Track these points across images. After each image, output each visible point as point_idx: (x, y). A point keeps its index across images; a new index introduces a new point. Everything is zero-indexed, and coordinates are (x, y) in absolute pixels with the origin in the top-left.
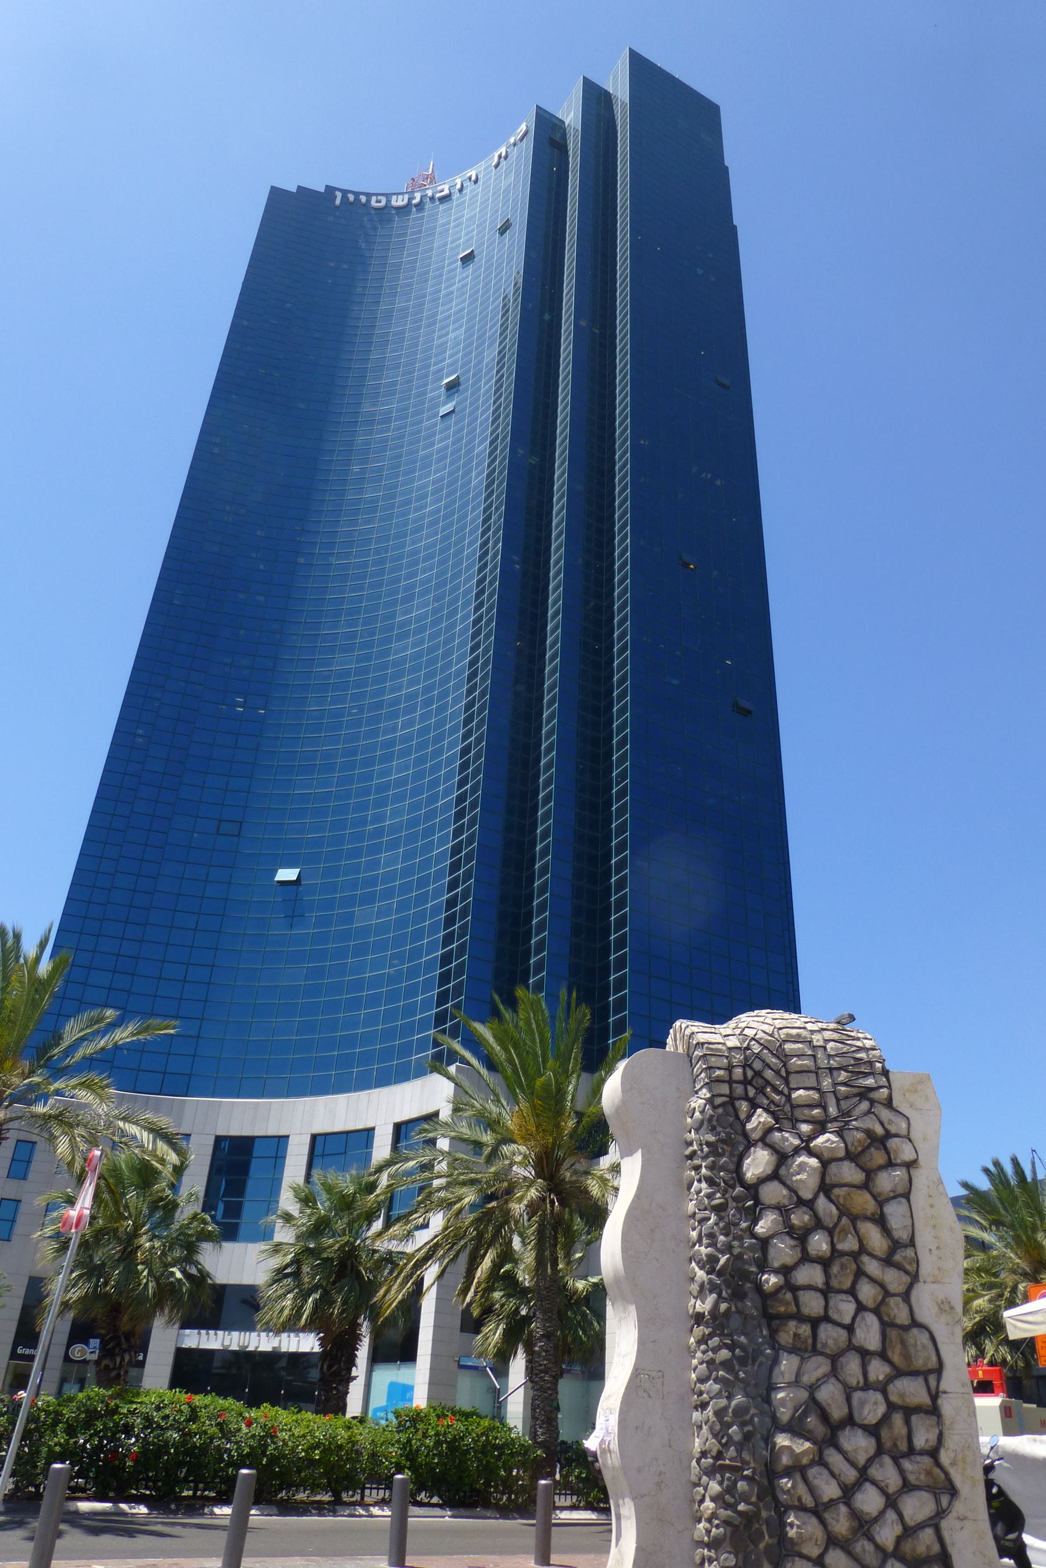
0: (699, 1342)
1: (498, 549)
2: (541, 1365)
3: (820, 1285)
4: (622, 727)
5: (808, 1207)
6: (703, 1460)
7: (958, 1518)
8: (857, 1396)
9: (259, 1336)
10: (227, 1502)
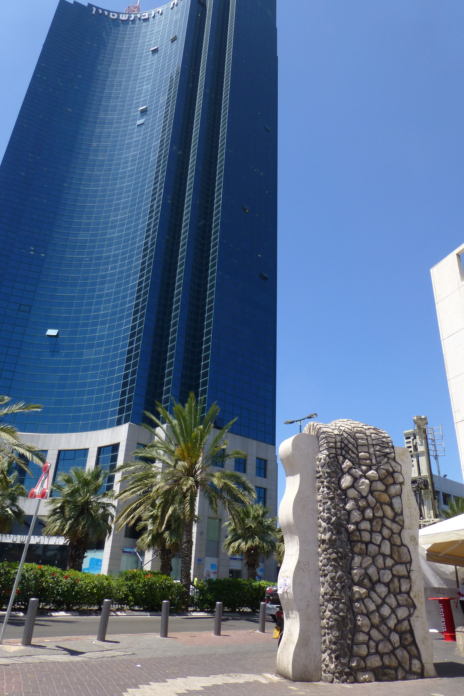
0: (323, 551)
1: (162, 192)
2: (185, 554)
3: (369, 529)
4: (212, 280)
6: (325, 596)
7: (416, 617)
8: (382, 572)
9: (44, 538)
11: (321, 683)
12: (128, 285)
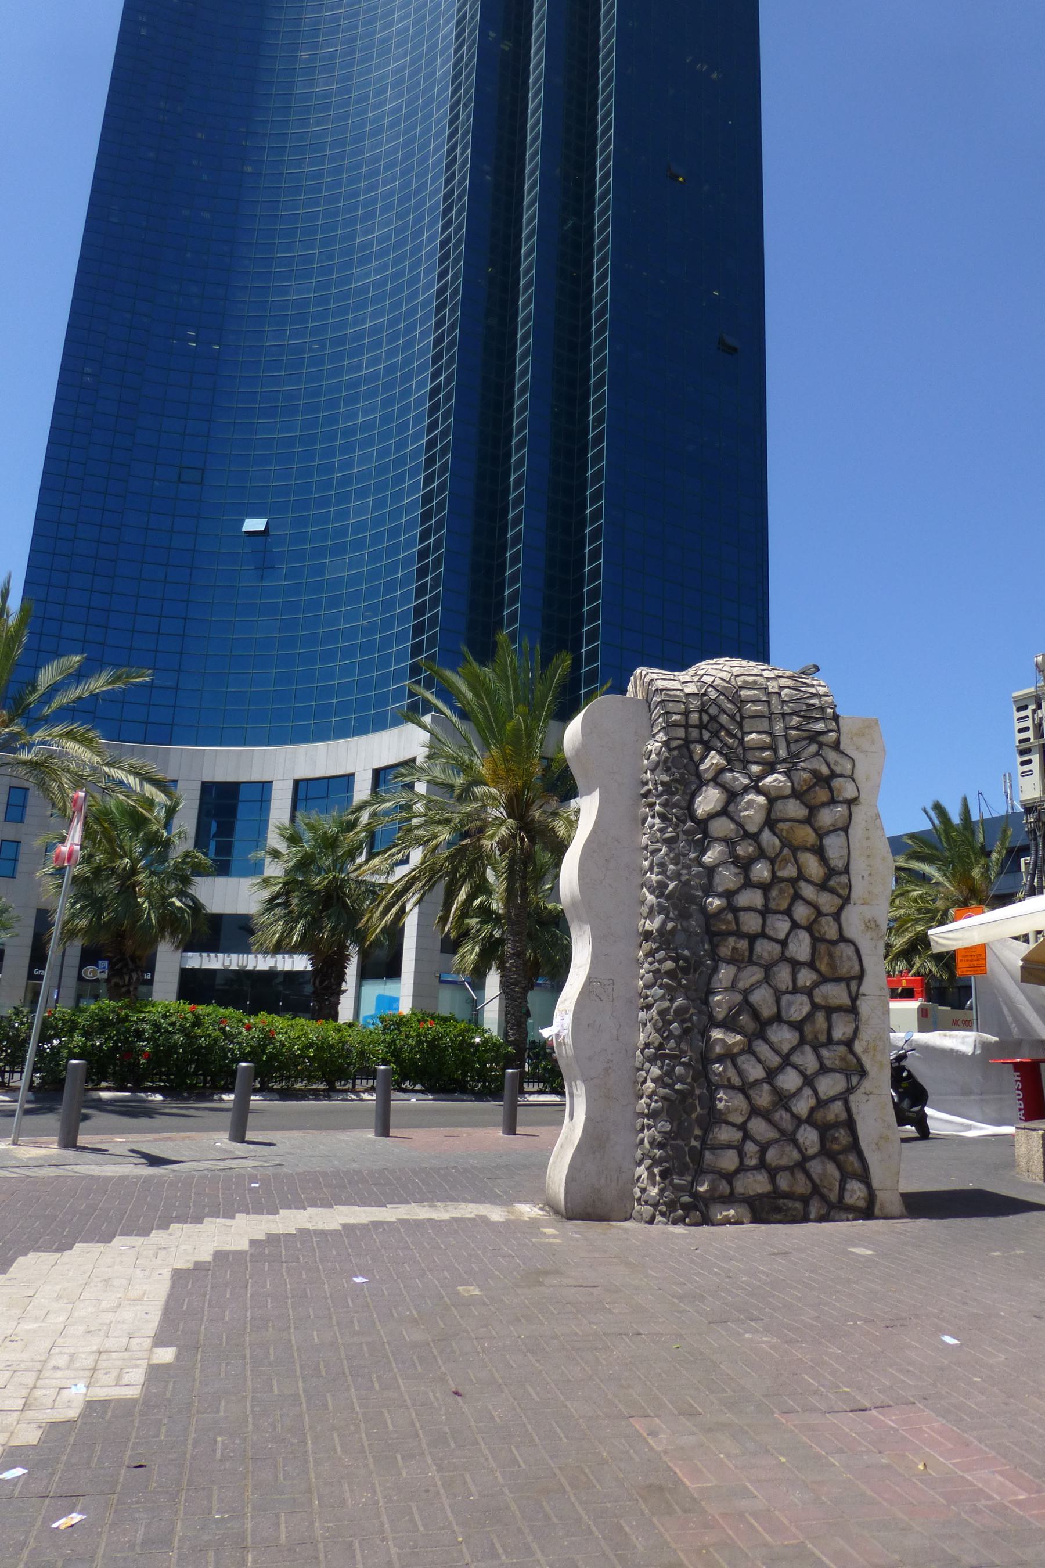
2: (512, 979)
4: (600, 366)
5: (753, 839)
9: (256, 957)
10: (231, 1091)
11: (627, 1224)
12: (408, 398)
